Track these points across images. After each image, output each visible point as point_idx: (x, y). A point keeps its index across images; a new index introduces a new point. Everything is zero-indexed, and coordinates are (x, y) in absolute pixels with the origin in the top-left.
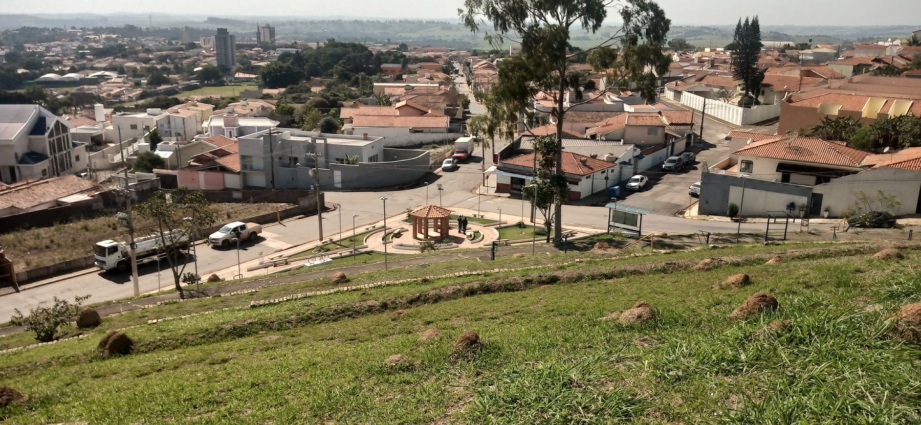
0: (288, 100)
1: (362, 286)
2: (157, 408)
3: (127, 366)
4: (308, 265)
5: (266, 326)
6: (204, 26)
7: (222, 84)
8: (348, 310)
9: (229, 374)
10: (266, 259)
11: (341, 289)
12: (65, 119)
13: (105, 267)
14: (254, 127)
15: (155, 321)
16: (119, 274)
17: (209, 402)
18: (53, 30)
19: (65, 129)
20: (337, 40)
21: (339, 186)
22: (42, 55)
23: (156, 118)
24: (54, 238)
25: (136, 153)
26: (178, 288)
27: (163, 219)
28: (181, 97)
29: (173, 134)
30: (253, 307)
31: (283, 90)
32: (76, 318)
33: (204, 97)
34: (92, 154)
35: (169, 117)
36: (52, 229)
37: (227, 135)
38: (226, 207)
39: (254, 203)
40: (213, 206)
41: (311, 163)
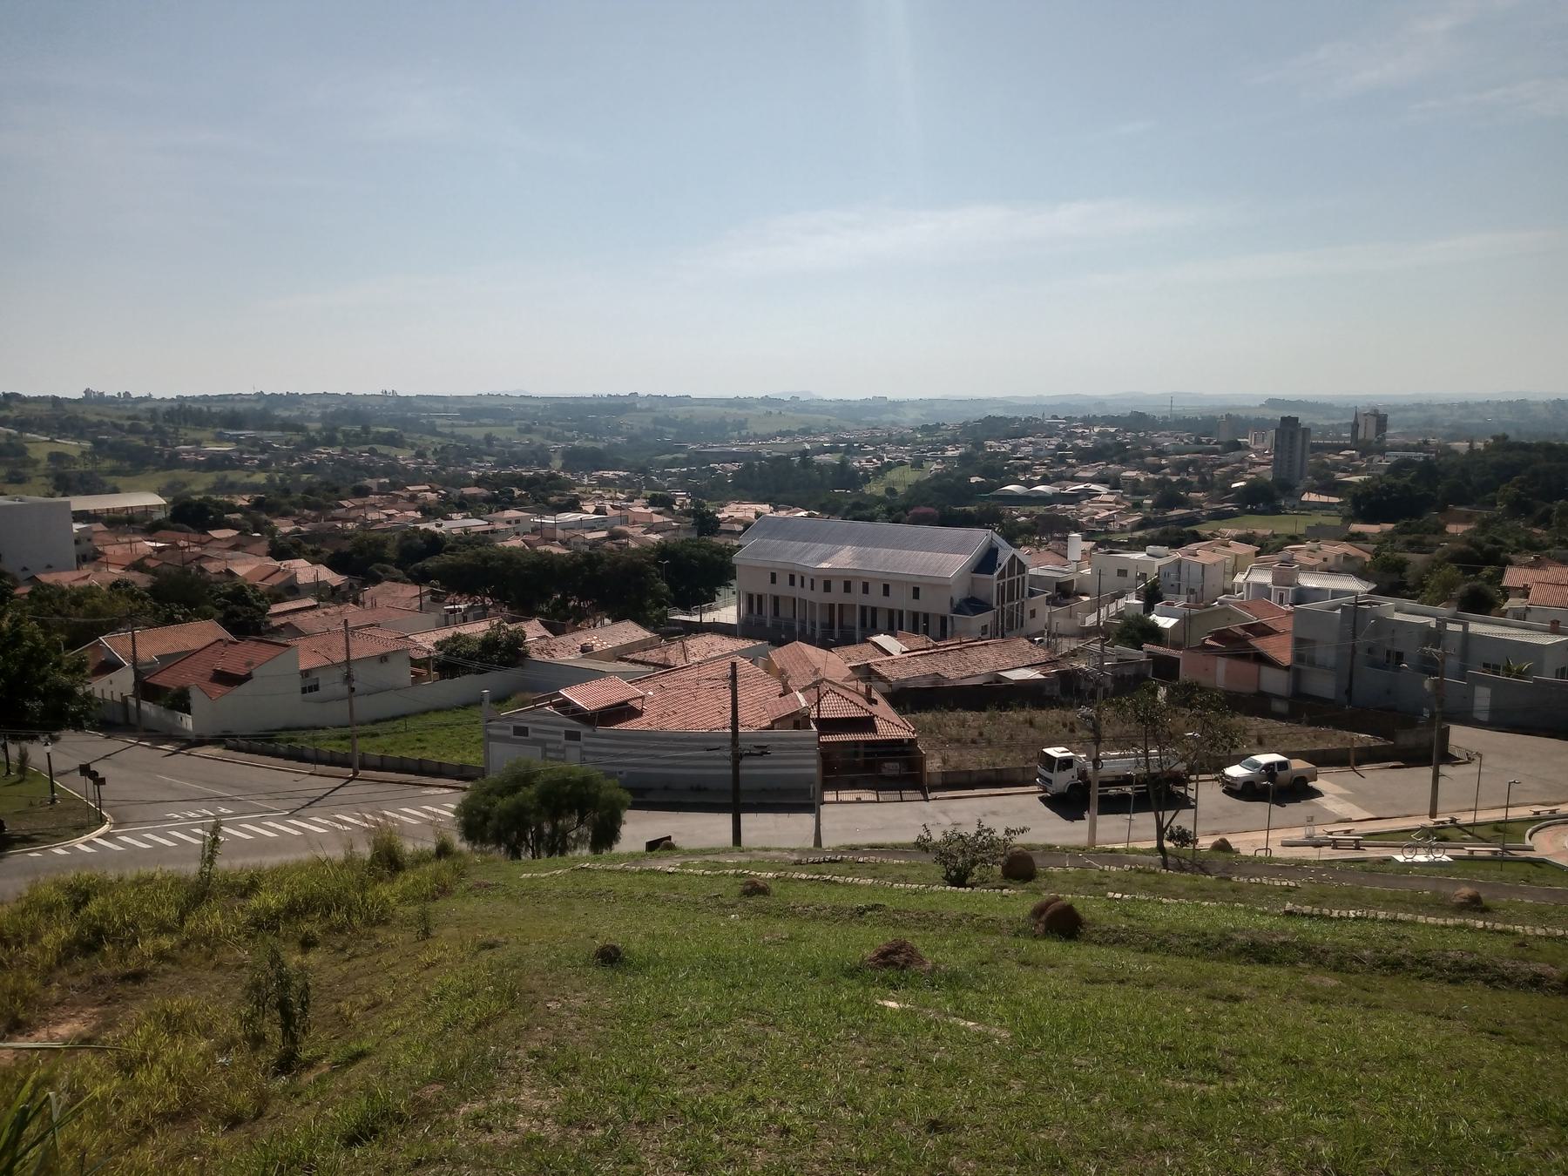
0: (1397, 545)
1: (1519, 928)
2: (1118, 1046)
3: (1071, 959)
4: (1400, 858)
5: (1312, 955)
6: (1259, 414)
7: (1277, 511)
8: (1485, 968)
9: (1242, 1025)
10: (1319, 832)
11: (1470, 922)
12: (1023, 553)
13: (1051, 789)
14: (1326, 590)
15: (1118, 896)
16: (1069, 804)
17: (1207, 1066)
18: (1027, 420)
19: (1023, 568)
20: (1513, 437)
21: (1484, 717)
22: (1006, 456)
23: (1158, 562)
24: (985, 730)
25: (1120, 615)
26: (1161, 848)
27: (1152, 729)
28: (1204, 530)
29: (1183, 589)
30: (1290, 913)
31: (1389, 527)
32: (1002, 860)
33: (1243, 532)
34: (1055, 609)
35: (1179, 561)
36: (984, 715)
37: (1274, 601)
38: (1256, 724)
39: (1310, 724)
40: (1239, 720)
41: (1429, 666)
